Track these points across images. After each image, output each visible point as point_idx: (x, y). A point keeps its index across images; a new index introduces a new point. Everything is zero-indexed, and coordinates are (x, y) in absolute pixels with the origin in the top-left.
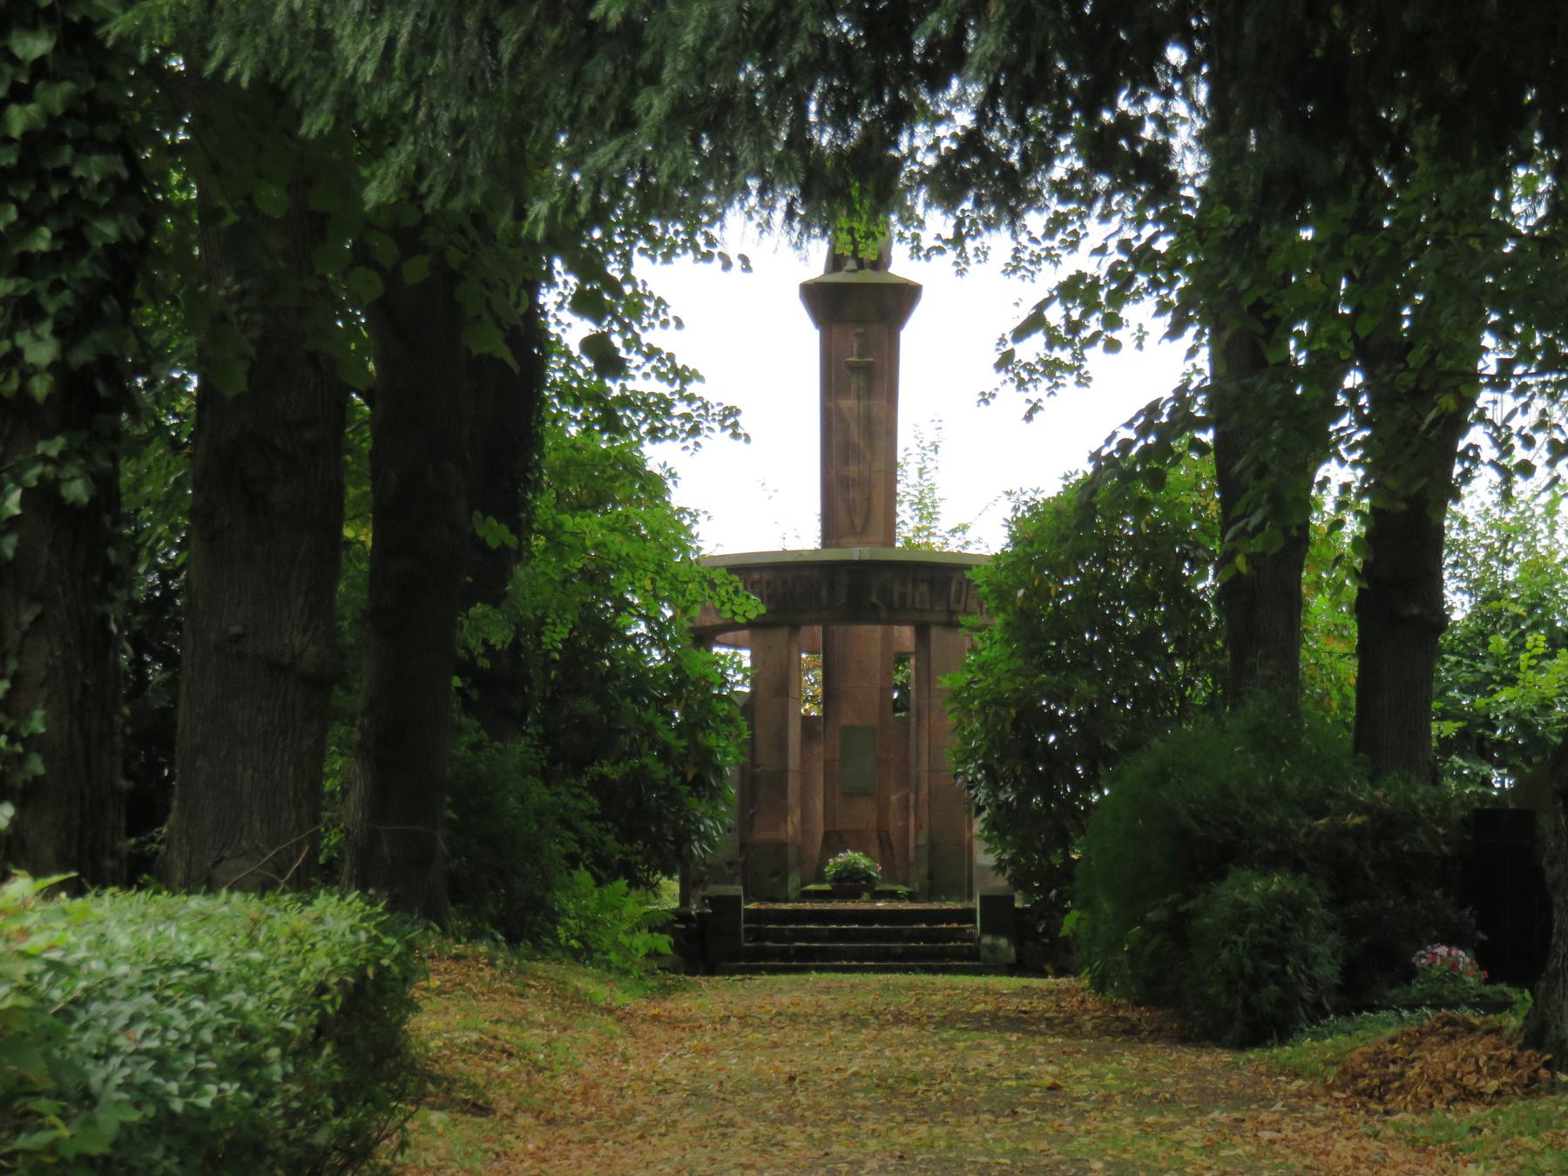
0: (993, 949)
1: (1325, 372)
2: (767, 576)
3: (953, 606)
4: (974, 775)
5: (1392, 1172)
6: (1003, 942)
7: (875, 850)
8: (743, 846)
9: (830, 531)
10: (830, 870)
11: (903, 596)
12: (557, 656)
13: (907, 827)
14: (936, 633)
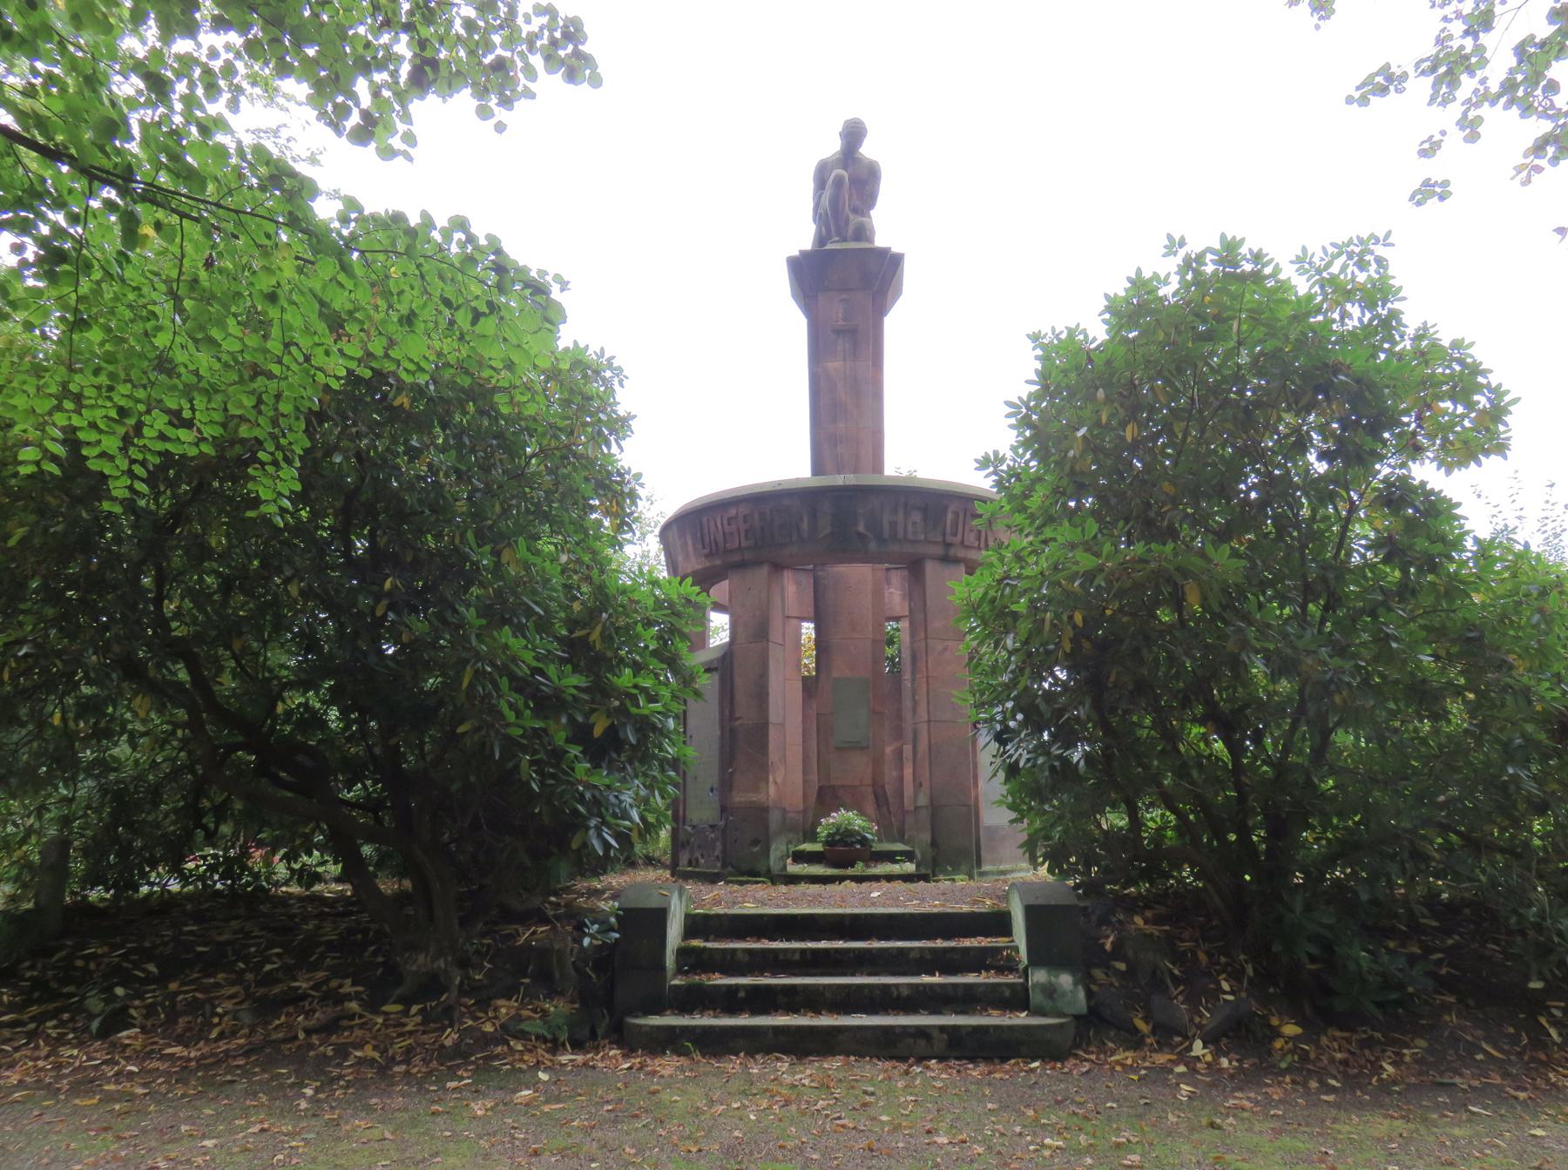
0: (1050, 991)
1: (1442, 806)
2: (744, 510)
3: (949, 539)
4: (1003, 722)
6: (1065, 980)
7: (870, 808)
8: (724, 809)
9: (818, 468)
10: (822, 832)
11: (893, 524)
13: (901, 779)
14: (930, 568)
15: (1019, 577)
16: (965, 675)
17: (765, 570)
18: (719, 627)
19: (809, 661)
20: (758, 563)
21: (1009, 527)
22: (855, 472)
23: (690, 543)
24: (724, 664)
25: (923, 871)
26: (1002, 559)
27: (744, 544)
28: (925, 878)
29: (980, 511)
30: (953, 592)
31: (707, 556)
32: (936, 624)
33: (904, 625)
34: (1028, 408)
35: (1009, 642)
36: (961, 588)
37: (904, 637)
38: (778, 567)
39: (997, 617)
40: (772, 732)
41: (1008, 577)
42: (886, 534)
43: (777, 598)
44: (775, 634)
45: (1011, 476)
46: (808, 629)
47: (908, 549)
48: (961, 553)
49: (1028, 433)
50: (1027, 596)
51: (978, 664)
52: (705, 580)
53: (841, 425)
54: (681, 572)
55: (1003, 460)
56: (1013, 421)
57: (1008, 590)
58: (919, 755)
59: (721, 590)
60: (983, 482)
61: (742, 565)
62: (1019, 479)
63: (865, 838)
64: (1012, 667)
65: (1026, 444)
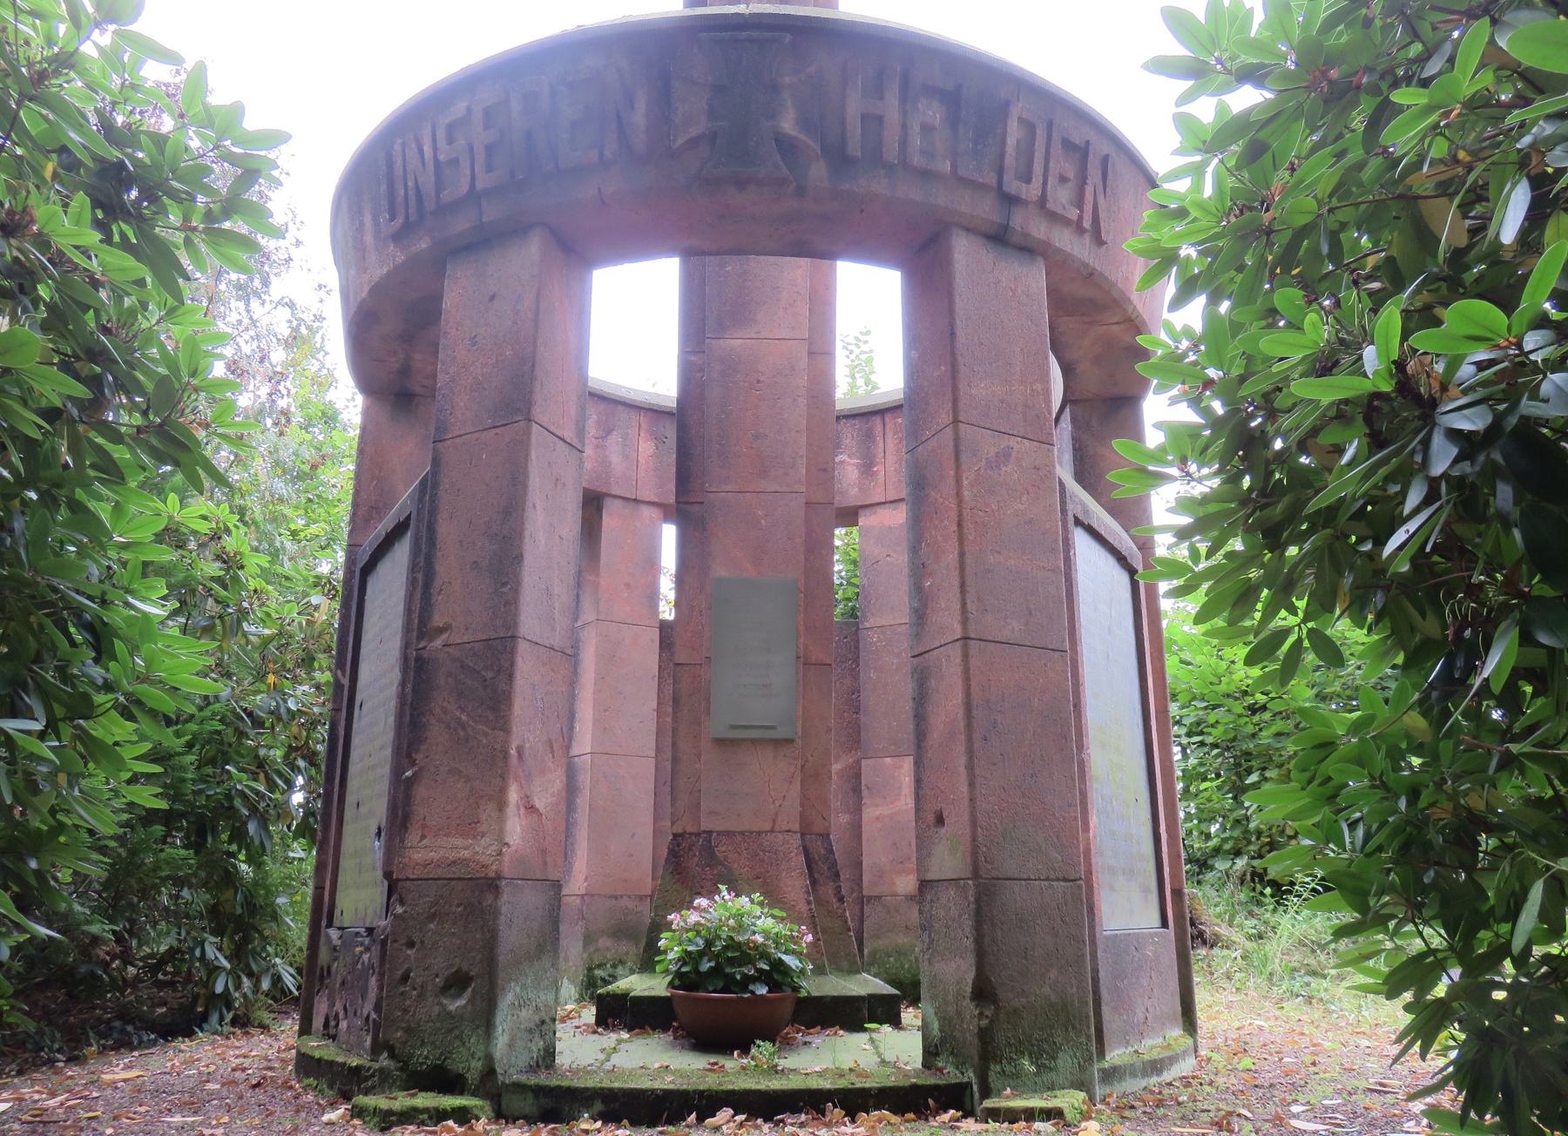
3: (1013, 186)
7: (794, 883)
10: (672, 949)
14: (964, 252)
17: (533, 249)
25: (951, 1074)
28: (956, 1099)
40: (528, 669)
42: (854, 148)
48: (1039, 229)
58: (936, 734)
63: (778, 965)
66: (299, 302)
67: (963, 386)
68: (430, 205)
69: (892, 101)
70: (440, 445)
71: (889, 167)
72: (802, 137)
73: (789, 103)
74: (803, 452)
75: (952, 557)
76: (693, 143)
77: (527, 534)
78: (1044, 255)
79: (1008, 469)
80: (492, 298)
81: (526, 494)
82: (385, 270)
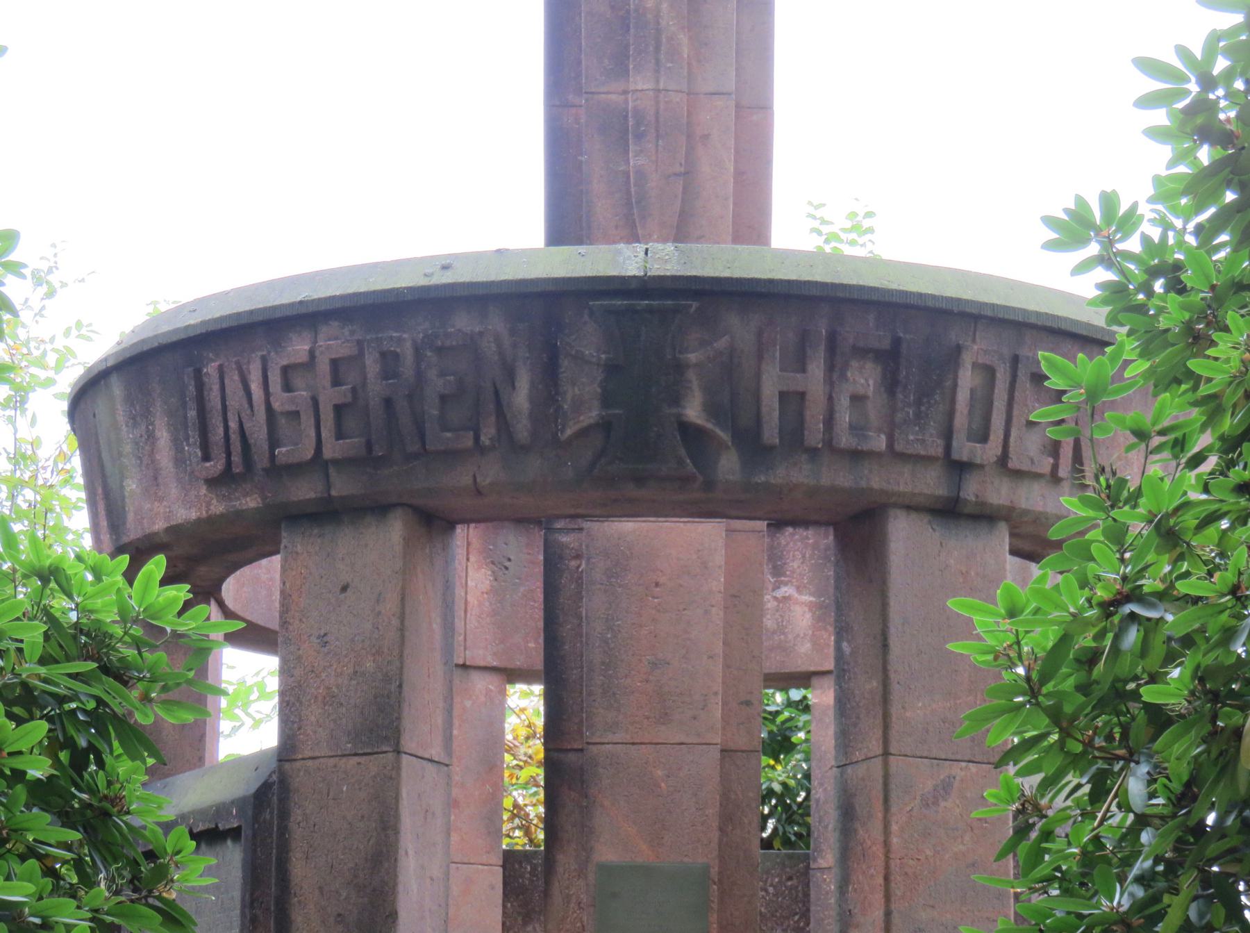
2: (334, 342)
3: (964, 449)
5: (4, 495)
9: (566, 223)
11: (793, 401)
12: (76, 806)
14: (905, 537)
15: (1165, 596)
16: (1005, 880)
17: (395, 530)
18: (247, 711)
19: (525, 795)
20: (372, 508)
21: (1141, 435)
22: (681, 233)
23: (163, 436)
24: (261, 821)
26: (1117, 536)
27: (332, 449)
29: (1055, 382)
30: (966, 629)
31: (212, 483)
32: (915, 709)
33: (822, 696)
34: (1208, 83)
35: (1136, 786)
36: (996, 613)
37: (818, 733)
38: (434, 522)
39: (1092, 709)
41: (1135, 595)
42: (771, 434)
43: (429, 625)
44: (421, 730)
45: (1154, 273)
46: (525, 704)
47: (838, 477)
48: (998, 493)
49: (1205, 155)
50: (1191, 659)
51: (1036, 856)
52: (201, 559)
53: (641, 82)
54: (133, 532)
55: (1129, 221)
56: (1160, 117)
57: (1132, 636)
59: (255, 585)
60: (1069, 283)
61: (326, 515)
62: (1177, 286)
64: (1142, 865)
65: (1201, 186)
66: (229, 739)
67: (895, 710)
68: (261, 461)
69: (816, 369)
70: (287, 766)
71: (813, 453)
72: (709, 426)
73: (695, 384)
74: (718, 687)
75: (879, 914)
76: (584, 433)
77: (400, 888)
78: (1007, 519)
79: (949, 804)
80: (344, 589)
81: (397, 840)
82: (193, 515)
